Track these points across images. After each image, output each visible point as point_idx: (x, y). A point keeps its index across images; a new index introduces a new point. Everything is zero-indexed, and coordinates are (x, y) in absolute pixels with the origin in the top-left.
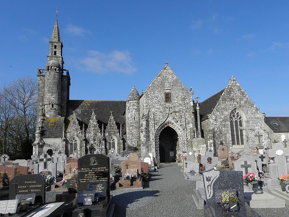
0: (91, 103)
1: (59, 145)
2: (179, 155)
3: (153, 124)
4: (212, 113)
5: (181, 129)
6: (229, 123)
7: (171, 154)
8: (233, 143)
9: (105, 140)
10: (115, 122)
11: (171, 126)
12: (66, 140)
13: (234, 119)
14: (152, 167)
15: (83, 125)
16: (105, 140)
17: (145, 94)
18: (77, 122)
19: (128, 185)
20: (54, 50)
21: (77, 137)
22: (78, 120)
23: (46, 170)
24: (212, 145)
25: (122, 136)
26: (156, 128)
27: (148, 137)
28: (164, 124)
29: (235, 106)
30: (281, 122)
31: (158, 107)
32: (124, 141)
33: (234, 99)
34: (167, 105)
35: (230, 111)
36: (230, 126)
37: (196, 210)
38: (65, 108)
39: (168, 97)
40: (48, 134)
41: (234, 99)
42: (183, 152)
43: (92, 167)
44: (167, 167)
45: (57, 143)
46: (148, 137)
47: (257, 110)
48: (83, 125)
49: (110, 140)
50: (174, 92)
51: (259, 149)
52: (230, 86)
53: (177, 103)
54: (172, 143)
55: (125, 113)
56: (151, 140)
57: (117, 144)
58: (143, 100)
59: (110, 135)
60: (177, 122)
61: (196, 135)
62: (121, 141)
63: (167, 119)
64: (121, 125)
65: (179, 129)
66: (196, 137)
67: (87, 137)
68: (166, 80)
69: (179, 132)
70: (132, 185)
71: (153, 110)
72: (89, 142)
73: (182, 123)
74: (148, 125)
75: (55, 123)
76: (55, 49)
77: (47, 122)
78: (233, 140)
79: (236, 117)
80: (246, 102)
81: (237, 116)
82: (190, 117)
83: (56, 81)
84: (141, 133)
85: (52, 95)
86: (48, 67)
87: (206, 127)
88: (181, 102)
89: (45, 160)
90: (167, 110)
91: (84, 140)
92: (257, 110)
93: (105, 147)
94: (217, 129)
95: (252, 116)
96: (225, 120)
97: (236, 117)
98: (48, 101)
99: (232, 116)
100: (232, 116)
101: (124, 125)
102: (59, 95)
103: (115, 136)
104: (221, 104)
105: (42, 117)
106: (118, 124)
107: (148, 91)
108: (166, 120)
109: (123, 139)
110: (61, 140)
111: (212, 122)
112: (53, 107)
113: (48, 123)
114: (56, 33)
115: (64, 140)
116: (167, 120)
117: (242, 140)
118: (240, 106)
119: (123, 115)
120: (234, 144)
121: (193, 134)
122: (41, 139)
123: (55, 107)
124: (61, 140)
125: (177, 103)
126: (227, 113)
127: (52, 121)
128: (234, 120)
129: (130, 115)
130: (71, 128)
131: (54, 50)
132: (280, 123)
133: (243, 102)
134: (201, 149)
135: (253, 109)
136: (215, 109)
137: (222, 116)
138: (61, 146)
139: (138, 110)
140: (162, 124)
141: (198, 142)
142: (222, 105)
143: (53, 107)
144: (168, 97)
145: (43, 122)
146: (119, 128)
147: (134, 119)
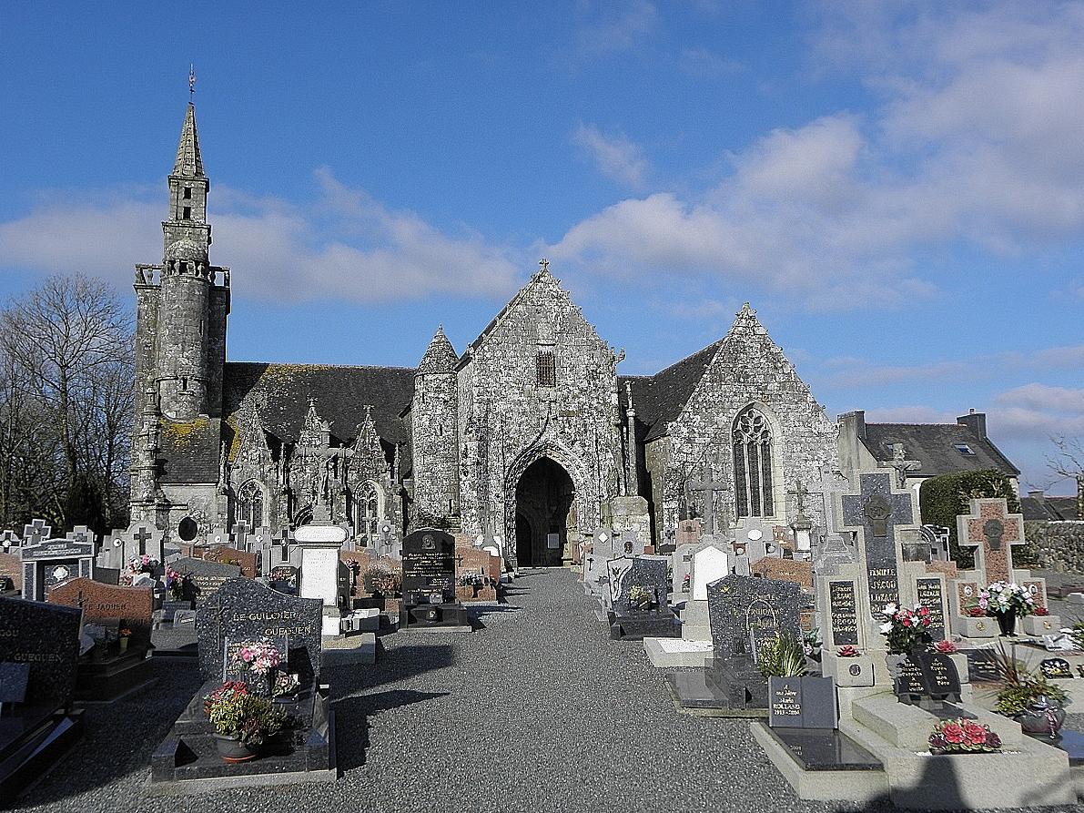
0: (297, 373)
1: (207, 507)
2: (576, 544)
3: (500, 451)
4: (679, 420)
5: (582, 465)
6: (731, 450)
7: (552, 541)
8: (742, 512)
9: (348, 493)
10: (378, 438)
11: (555, 457)
12: (228, 492)
13: (745, 438)
14: (503, 573)
15: (281, 447)
16: (348, 493)
17: (476, 356)
18: (263, 437)
19: (469, 596)
20: (185, 203)
21: (261, 484)
22: (265, 432)
23: (286, 564)
24: (676, 516)
25: (401, 482)
26: (511, 458)
27: (483, 489)
28: (532, 451)
29: (750, 398)
30: (916, 444)
31: (516, 397)
32: (406, 499)
33: (748, 376)
34: (543, 391)
35: (734, 413)
36: (731, 460)
37: (597, 621)
38: (219, 389)
39: (545, 370)
40: (174, 472)
41: (748, 376)
42: (587, 535)
43: (427, 551)
44: (536, 580)
45: (202, 501)
46: (483, 489)
47: (817, 410)
48: (281, 447)
49: (362, 494)
50: (566, 353)
51: (799, 529)
52: (736, 336)
53: (573, 385)
54: (555, 508)
55: (408, 409)
56: (492, 497)
57: (383, 505)
58: (469, 375)
59: (362, 478)
60: (573, 444)
61: (622, 487)
62: (398, 499)
63: (541, 434)
64: (395, 447)
65: (578, 467)
66: (623, 493)
67: (292, 484)
68: (541, 315)
69: (578, 477)
70: (475, 596)
71: (501, 407)
72: (296, 500)
73: (586, 449)
74: (483, 452)
75: (193, 438)
76: (186, 200)
77: (171, 433)
78: (741, 501)
79: (751, 431)
80: (783, 386)
81: (757, 429)
82: (605, 428)
83: (196, 305)
84: (462, 476)
85: (183, 350)
86: (173, 262)
87: (659, 460)
88: (585, 384)
89: (283, 542)
90: (542, 406)
91: (284, 493)
92: (817, 410)
93: (347, 515)
94: (692, 467)
95: (802, 429)
96: (717, 440)
97: (751, 431)
98: (172, 367)
99: (739, 427)
100: (739, 427)
101: (406, 443)
102: (203, 351)
103: (378, 481)
104: (706, 390)
105: (154, 419)
106: (388, 448)
107: (486, 348)
108: (538, 438)
109: (403, 493)
110: (214, 490)
111: (679, 445)
112: (185, 387)
113: (172, 438)
114: (189, 149)
115: (226, 492)
116: (543, 438)
117: (769, 502)
118: (767, 398)
119: (402, 416)
120: (743, 515)
121: (616, 485)
122: (157, 487)
123: (193, 386)
124: (214, 490)
125: (573, 385)
126: (725, 419)
127: (185, 431)
128: (746, 438)
129: (423, 419)
130: (245, 454)
131: (185, 203)
132: (911, 444)
133: (773, 386)
134: (636, 527)
135: (803, 405)
136: (688, 408)
137: (710, 430)
138: (214, 507)
139: (452, 404)
140: (526, 450)
141: (627, 506)
142: (710, 394)
143: (185, 387)
144: (545, 370)
145: (157, 434)
146: (390, 459)
147: (439, 433)
